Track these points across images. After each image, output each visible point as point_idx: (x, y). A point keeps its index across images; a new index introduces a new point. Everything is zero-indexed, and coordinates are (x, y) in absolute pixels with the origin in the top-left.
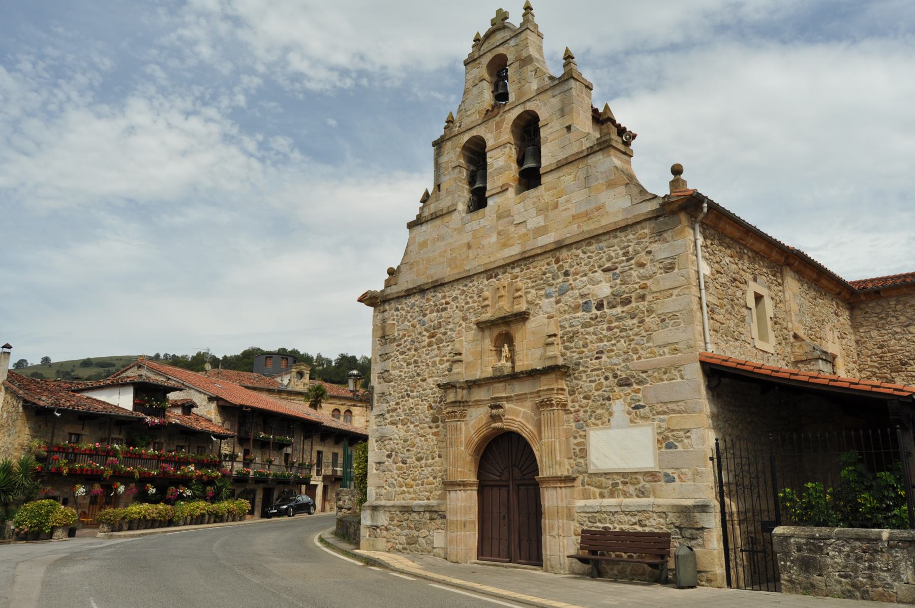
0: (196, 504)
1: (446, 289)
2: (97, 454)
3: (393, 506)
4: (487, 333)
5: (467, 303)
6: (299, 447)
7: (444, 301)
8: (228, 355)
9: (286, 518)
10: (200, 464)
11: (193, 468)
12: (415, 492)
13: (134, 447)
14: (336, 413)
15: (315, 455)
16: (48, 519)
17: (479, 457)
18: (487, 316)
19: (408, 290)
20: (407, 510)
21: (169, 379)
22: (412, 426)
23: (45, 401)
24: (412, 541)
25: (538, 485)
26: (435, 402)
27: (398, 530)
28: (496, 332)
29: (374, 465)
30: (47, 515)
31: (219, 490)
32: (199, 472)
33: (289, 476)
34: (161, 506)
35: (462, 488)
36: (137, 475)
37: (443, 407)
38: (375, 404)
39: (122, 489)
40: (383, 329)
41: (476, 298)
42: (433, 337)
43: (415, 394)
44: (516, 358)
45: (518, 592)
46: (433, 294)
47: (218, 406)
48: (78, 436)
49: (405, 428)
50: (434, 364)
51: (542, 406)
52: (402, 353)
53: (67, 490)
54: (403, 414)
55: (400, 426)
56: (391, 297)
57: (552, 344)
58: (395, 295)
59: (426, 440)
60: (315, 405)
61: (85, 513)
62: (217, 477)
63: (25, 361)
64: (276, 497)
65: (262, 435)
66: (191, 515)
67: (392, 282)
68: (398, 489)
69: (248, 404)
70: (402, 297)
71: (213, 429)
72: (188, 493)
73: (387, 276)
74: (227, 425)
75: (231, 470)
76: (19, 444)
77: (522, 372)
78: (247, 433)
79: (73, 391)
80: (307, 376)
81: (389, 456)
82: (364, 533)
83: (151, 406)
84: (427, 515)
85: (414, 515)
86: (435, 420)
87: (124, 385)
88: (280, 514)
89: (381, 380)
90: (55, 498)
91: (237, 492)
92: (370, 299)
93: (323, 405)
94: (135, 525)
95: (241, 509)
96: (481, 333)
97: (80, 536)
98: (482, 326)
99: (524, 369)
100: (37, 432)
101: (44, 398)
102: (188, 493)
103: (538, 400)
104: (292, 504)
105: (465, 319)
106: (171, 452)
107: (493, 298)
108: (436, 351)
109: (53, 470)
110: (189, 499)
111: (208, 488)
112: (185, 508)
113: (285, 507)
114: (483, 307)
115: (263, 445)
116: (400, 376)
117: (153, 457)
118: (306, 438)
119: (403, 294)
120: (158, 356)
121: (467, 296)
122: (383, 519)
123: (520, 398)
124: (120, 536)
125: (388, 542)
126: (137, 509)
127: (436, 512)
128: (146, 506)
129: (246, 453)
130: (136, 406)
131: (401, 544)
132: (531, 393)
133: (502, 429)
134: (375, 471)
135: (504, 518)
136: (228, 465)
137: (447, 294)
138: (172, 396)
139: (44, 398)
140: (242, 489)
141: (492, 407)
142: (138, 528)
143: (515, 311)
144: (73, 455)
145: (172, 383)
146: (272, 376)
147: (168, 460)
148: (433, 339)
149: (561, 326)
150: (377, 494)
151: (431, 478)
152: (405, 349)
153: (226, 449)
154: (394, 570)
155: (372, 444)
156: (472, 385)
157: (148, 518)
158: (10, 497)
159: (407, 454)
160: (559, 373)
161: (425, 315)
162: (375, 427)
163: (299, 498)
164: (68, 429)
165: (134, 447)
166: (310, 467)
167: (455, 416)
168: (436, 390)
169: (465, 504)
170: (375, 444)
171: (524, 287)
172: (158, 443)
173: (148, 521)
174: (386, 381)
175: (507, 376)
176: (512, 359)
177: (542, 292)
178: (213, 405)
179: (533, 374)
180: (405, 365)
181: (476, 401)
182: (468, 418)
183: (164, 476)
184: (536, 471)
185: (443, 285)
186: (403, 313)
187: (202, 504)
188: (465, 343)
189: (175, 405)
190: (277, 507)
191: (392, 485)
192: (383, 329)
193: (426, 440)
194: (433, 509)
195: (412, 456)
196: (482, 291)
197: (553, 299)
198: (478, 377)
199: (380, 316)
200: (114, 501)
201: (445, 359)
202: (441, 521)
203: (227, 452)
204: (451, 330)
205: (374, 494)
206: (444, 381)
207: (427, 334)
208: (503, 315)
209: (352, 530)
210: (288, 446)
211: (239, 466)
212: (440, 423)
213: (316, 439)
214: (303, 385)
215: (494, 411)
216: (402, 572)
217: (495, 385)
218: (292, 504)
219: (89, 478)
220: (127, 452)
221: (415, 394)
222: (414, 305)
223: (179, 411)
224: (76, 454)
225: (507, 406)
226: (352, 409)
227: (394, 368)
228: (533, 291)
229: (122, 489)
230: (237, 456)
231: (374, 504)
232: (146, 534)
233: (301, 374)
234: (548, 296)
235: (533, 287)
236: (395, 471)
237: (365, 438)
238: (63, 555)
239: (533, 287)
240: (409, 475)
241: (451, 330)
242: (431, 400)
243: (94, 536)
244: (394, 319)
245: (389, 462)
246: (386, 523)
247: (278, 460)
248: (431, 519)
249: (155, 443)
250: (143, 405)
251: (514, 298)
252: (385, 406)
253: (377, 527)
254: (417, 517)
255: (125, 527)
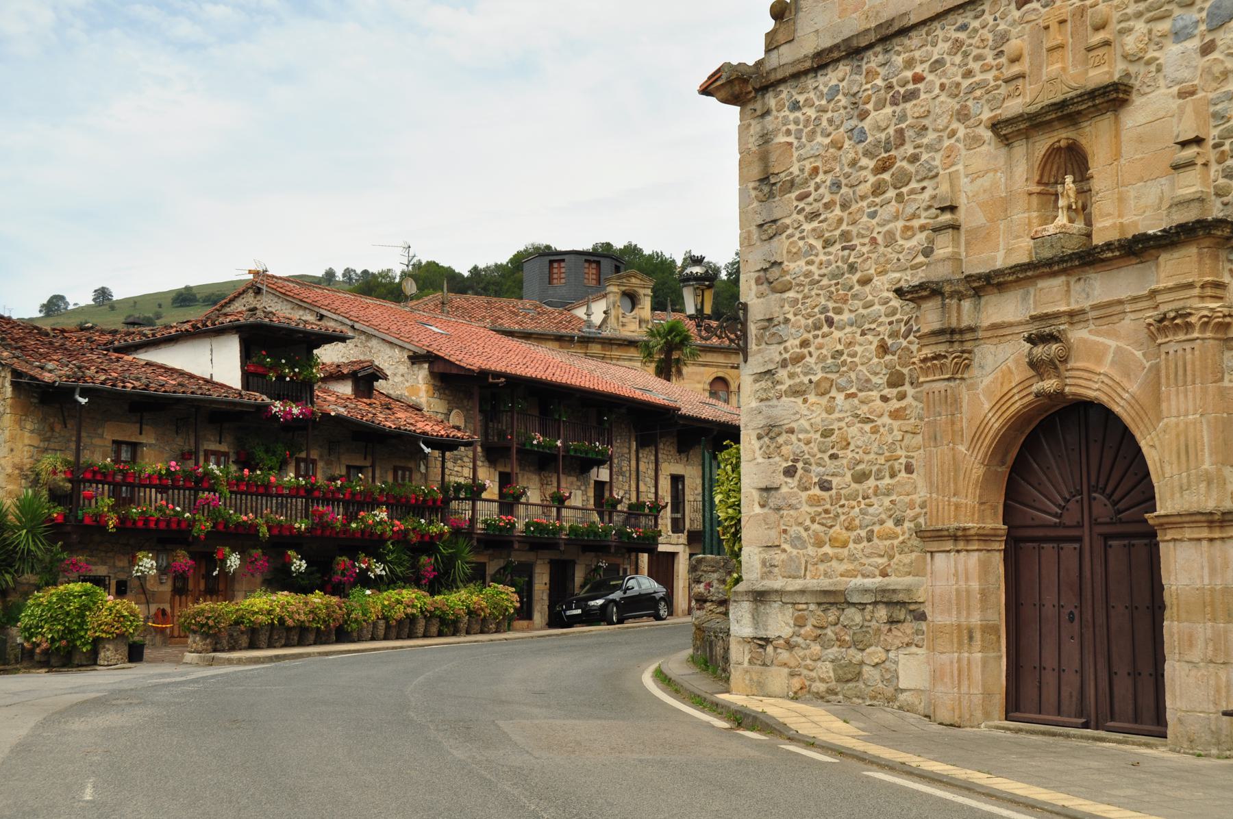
0: (393, 594)
1: (914, 40)
2: (175, 487)
3: (802, 592)
4: (1020, 149)
5: (968, 74)
6: (628, 465)
7: (909, 74)
8: (481, 266)
9: (603, 628)
10: (401, 506)
11: (384, 515)
12: (852, 558)
13: (252, 470)
14: (719, 386)
15: (665, 485)
16: (84, 622)
17: (1004, 470)
18: (1014, 107)
19: (818, 55)
20: (833, 600)
21: (322, 317)
22: (840, 397)
23: (53, 372)
24: (850, 674)
25: (1154, 535)
26: (894, 335)
27: (816, 648)
28: (1042, 144)
29: (756, 495)
30: (82, 616)
31: (450, 561)
32: (399, 525)
33: (606, 532)
34: (317, 598)
35: (949, 545)
36: (264, 530)
37: (914, 348)
38: (753, 346)
39: (234, 561)
40: (764, 158)
41: (990, 60)
42: (884, 169)
43: (846, 316)
44: (1095, 210)
45: (1078, 795)
46: (881, 58)
47: (432, 373)
48: (134, 447)
49: (824, 401)
50: (890, 239)
51: (1163, 330)
52: (814, 216)
53: (122, 563)
54: (818, 368)
55: (812, 398)
56: (779, 75)
57: (1190, 164)
58: (789, 71)
59: (875, 431)
60: (666, 370)
61: (164, 612)
62: (442, 534)
63: (62, 298)
64: (583, 580)
65: (538, 439)
66: (385, 618)
67: (781, 38)
68: (811, 550)
69: (500, 367)
70: (805, 73)
71: (422, 426)
72: (379, 570)
73: (770, 24)
74: (456, 418)
75: (473, 520)
76: (15, 466)
77: (1108, 246)
78: (502, 434)
79: (117, 350)
80: (647, 303)
81: (790, 472)
82: (739, 654)
83: (281, 378)
84: (882, 613)
85: (851, 611)
86: (895, 381)
87: (219, 332)
88: (591, 618)
89: (765, 286)
90: (98, 581)
91: (491, 569)
92: (734, 86)
93: (685, 370)
94: (263, 638)
95: (496, 606)
96: (1004, 151)
97: (154, 661)
98: (1008, 131)
99: (1113, 236)
100: (48, 440)
101: (50, 366)
102: (379, 570)
103: (1151, 315)
104: (617, 595)
105: (963, 115)
106: (334, 479)
107: (1035, 53)
108: (893, 207)
109: (87, 521)
110: (378, 584)
111: (424, 559)
112: (372, 602)
113: (600, 602)
114: (1007, 81)
115: (544, 462)
116: (808, 274)
117: (296, 492)
118: (642, 445)
119: (808, 65)
120: (330, 275)
121: (966, 55)
122: (779, 623)
123: (1108, 311)
124: (230, 662)
125: (792, 675)
126: (262, 603)
127: (903, 604)
128: (283, 597)
129: (505, 480)
130: (247, 377)
131: (822, 680)
132: (1135, 299)
133: (1059, 395)
134: (758, 510)
135: (1072, 620)
136: (462, 509)
137: (917, 54)
138: (328, 355)
139: (50, 366)
140: (502, 563)
141: (1032, 340)
142: (270, 646)
143: (1091, 85)
144: (125, 485)
145: (331, 326)
146: (566, 305)
147: (330, 498)
148: (886, 176)
149: (1215, 115)
150: (764, 563)
151: (890, 524)
152: (818, 206)
153: (459, 473)
154: (794, 738)
155: (749, 444)
156: (987, 284)
157: (290, 622)
158: (8, 577)
159: (831, 466)
160: (1207, 242)
161: (863, 116)
162: (754, 404)
163: (631, 583)
164: (110, 433)
165: (252, 470)
166: (656, 508)
167: (942, 369)
168: (896, 302)
169: (965, 583)
170: (756, 444)
171: (1116, 16)
172: (304, 460)
173: (289, 629)
174: (774, 291)
175: (1071, 257)
176: (1082, 210)
177: (1164, 26)
178: (422, 372)
179: (1138, 248)
180: (818, 244)
181: (994, 327)
182: (975, 371)
183: (321, 528)
184: (1149, 500)
185: (904, 31)
186: (812, 113)
187: (408, 594)
188: (964, 181)
189: (336, 375)
190: (582, 602)
191: (798, 542)
192: (764, 158)
193: (875, 431)
194: (895, 598)
195: (849, 477)
196: (1004, 38)
197: (1194, 44)
198: (999, 264)
199: (756, 128)
200: (220, 587)
201: (916, 223)
202: (915, 625)
203: (462, 480)
204: (930, 148)
205: (758, 564)
206: (910, 279)
207: (871, 164)
208: (1059, 98)
209: (719, 650)
210: (599, 463)
211: (487, 510)
212: (907, 387)
213: (667, 450)
214: (637, 322)
215: (1039, 351)
216: (811, 744)
217: (1042, 284)
218: (617, 595)
219: (164, 537)
220: (240, 480)
221: (846, 316)
222: (835, 90)
223: (346, 389)
224: (132, 486)
225: (1078, 335)
226: (728, 374)
227: (795, 256)
228: (1140, 26)
229: (234, 561)
230: (483, 488)
231: (758, 587)
232: (285, 657)
233: (632, 299)
234: (1179, 35)
235: (1139, 15)
236: (805, 508)
237: (731, 433)
238: (93, 695)
239: (1139, 15)
240: (837, 515)
241: (930, 148)
242: (884, 330)
243: (178, 661)
244: (788, 133)
245: (789, 486)
246: (787, 632)
247: (579, 497)
248: (892, 622)
249: (298, 461)
250: (264, 376)
251: (1089, 49)
252: (774, 353)
253: (767, 640)
254: (858, 618)
255: (244, 640)
